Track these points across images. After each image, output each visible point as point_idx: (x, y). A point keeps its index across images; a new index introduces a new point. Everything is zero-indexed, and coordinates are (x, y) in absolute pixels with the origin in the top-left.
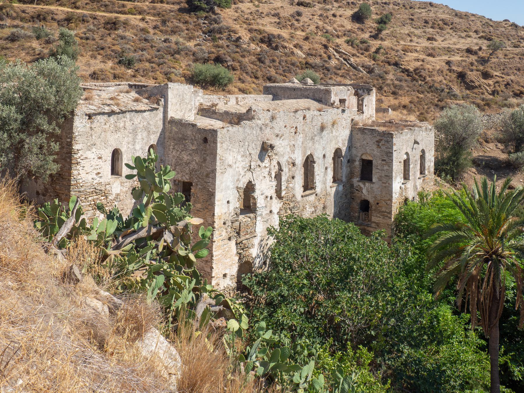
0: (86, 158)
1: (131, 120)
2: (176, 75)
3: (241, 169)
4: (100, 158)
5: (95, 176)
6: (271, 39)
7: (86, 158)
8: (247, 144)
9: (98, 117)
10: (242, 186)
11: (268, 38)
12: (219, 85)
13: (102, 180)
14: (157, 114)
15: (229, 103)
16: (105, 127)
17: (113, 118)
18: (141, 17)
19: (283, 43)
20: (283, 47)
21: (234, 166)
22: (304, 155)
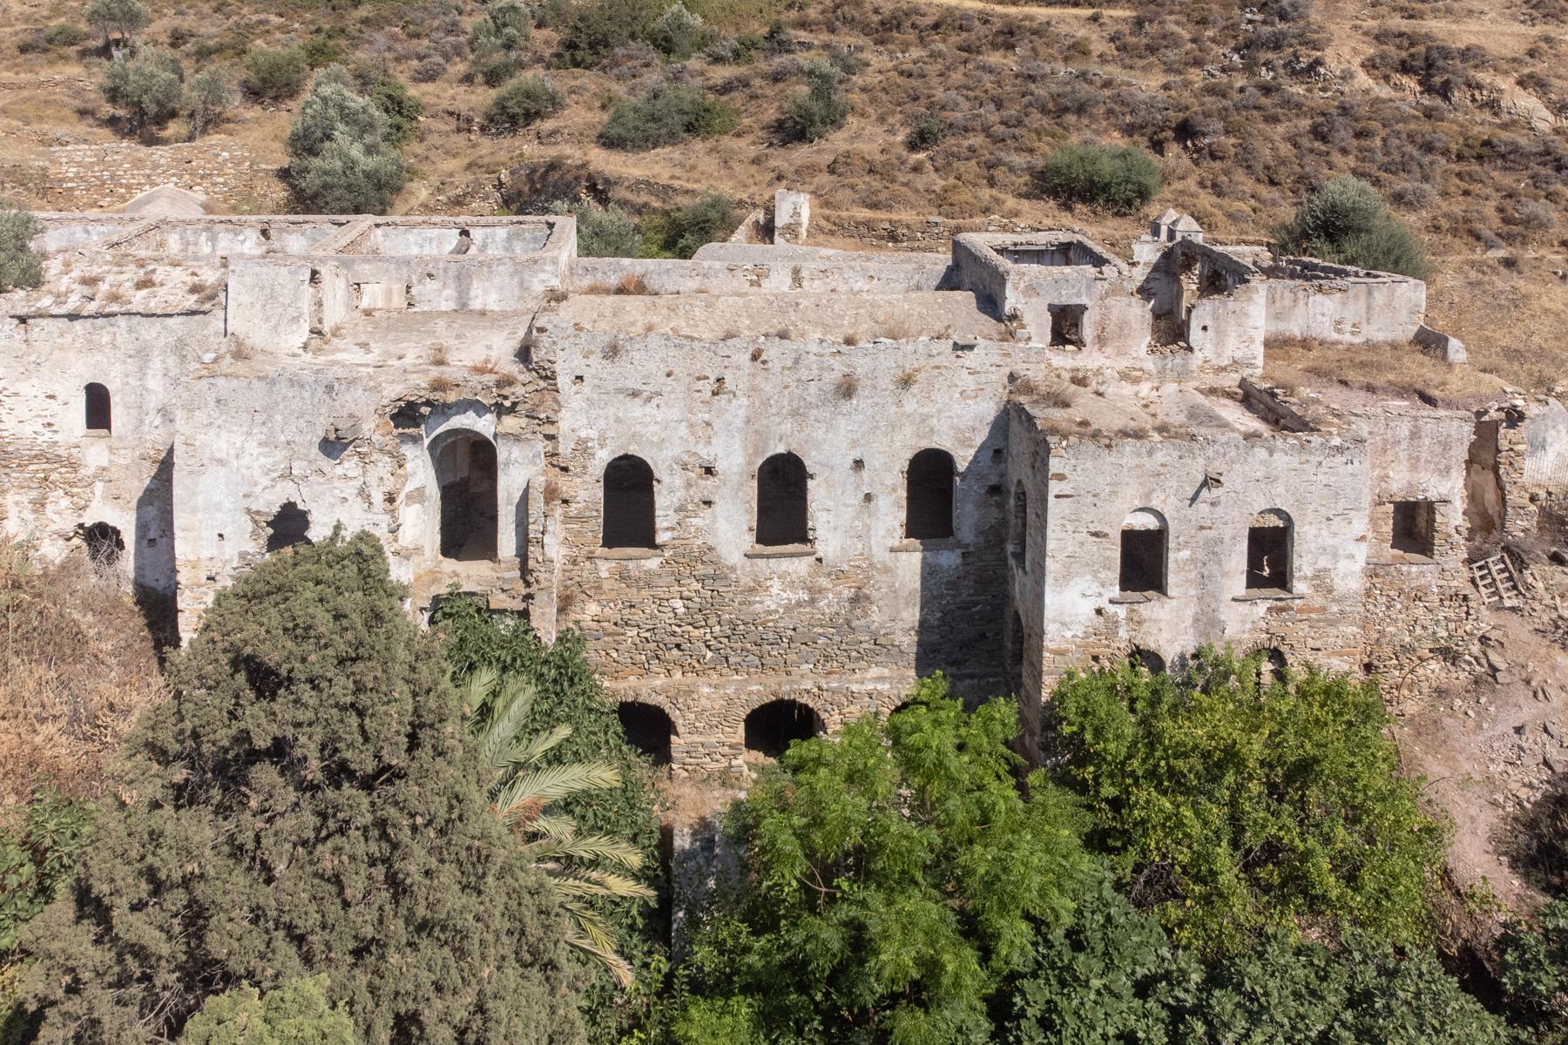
0: (16, 394)
1: (130, 331)
2: (1011, 169)
3: (257, 473)
4: (52, 397)
5: (41, 429)
6: (1434, 61)
7: (16, 394)
8: (278, 418)
9: (43, 322)
10: (264, 509)
11: (1427, 59)
12: (1107, 201)
13: (56, 438)
14: (206, 325)
15: (765, 283)
16: (60, 341)
17: (78, 324)
18: (1090, 12)
19: (1472, 72)
20: (1469, 86)
21: (235, 463)
22: (756, 453)
